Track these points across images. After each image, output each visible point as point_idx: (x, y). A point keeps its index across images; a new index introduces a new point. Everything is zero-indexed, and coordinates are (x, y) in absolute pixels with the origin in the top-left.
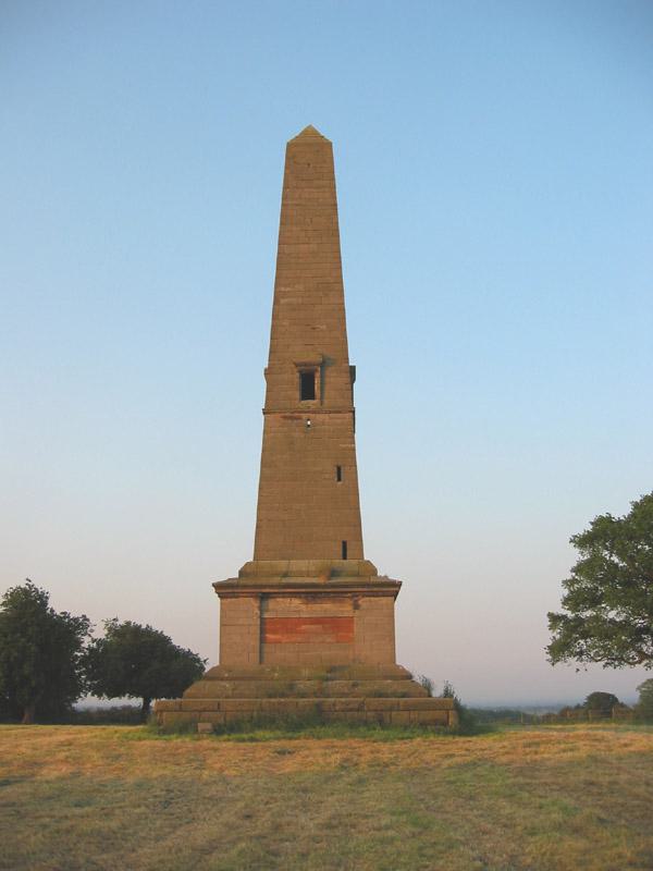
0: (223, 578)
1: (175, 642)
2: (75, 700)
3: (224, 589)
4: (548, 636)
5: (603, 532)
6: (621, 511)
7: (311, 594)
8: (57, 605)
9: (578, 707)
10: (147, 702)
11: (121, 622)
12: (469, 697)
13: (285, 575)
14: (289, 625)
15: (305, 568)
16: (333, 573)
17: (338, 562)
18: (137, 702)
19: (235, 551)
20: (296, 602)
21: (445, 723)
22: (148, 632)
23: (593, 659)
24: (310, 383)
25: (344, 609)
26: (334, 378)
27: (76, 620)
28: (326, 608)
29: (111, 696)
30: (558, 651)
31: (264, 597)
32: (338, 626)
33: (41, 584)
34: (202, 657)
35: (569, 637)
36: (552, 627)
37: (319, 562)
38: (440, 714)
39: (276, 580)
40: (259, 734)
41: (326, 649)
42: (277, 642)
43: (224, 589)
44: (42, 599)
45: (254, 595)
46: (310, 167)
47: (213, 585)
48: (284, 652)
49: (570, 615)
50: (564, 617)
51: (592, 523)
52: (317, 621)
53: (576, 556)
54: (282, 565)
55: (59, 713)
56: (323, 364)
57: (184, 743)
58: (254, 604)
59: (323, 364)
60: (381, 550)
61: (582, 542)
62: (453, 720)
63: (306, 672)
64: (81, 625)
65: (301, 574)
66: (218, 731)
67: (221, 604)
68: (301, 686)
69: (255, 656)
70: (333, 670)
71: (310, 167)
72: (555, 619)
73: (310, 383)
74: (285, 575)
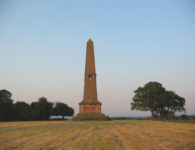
0: (79, 102)
1: (68, 106)
2: (50, 117)
3: (80, 104)
4: (131, 106)
5: (140, 89)
6: (143, 86)
7: (90, 104)
8: (48, 101)
9: (150, 117)
10: (63, 117)
11: (58, 102)
12: (110, 116)
13: (87, 102)
14: (88, 108)
15: (90, 101)
16: (93, 102)
17: (94, 100)
18: (62, 117)
19: (81, 99)
20: (89, 105)
21: (106, 119)
22: (63, 104)
23: (138, 110)
24: (90, 75)
25: (94, 106)
26: (93, 76)
27: (52, 103)
28: (92, 106)
29: (56, 116)
30: (133, 108)
31: (85, 105)
32: (94, 108)
33: (45, 97)
34: (74, 108)
35: (134, 107)
36: (131, 105)
37: (92, 100)
38: (105, 118)
39: (86, 103)
40: (84, 121)
41: (92, 111)
42: (86, 110)
43: (80, 104)
44: (46, 100)
45: (84, 105)
46: (90, 45)
47: (79, 104)
48: (87, 111)
49: (135, 103)
50: (133, 103)
51: (135, 92)
52: (90, 108)
53: (134, 94)
54: (87, 101)
55: (48, 119)
56: (92, 75)
57: (76, 122)
58: (84, 106)
59: (92, 75)
60: (99, 99)
61: (135, 92)
62: (107, 119)
63: (90, 114)
64: (52, 104)
65: (89, 102)
66: (80, 120)
67: (80, 106)
68: (89, 115)
69: (84, 112)
70: (93, 113)
71: (90, 45)
72: (132, 104)
73: (90, 75)
74: (87, 102)
